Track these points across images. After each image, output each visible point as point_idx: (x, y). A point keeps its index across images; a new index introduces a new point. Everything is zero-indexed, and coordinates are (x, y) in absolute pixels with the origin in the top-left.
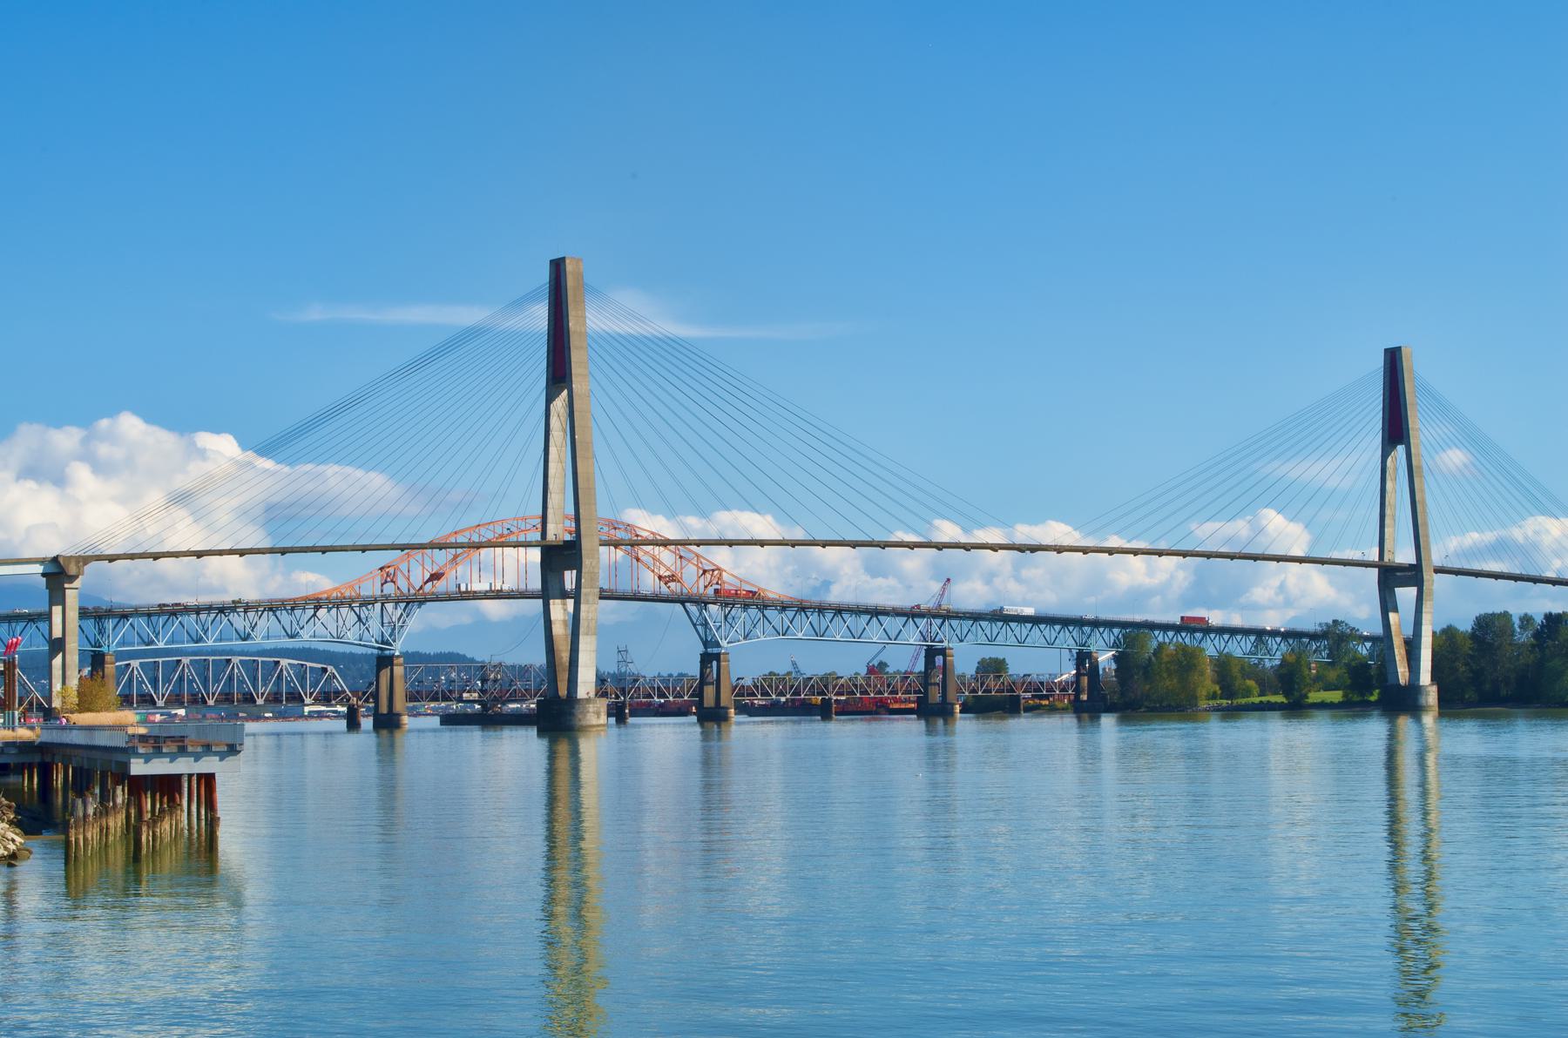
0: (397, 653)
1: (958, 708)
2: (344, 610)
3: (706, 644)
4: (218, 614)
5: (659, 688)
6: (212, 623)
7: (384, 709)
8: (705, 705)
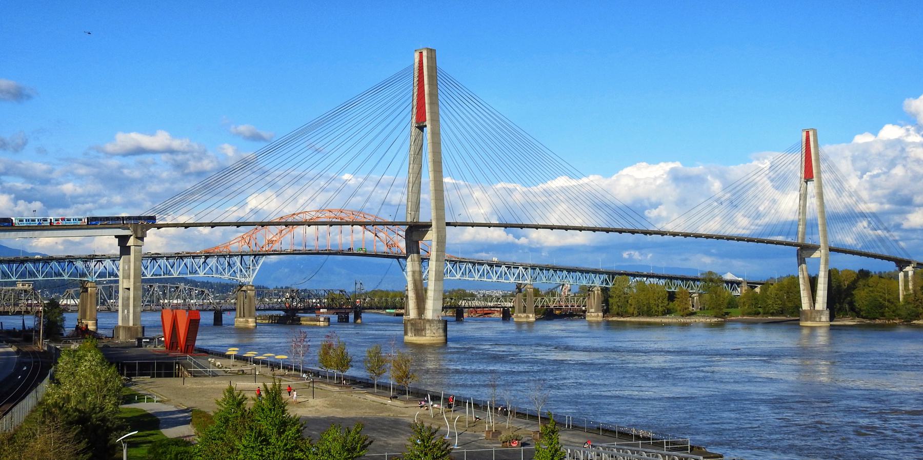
2: (222, 260)
4: (152, 260)
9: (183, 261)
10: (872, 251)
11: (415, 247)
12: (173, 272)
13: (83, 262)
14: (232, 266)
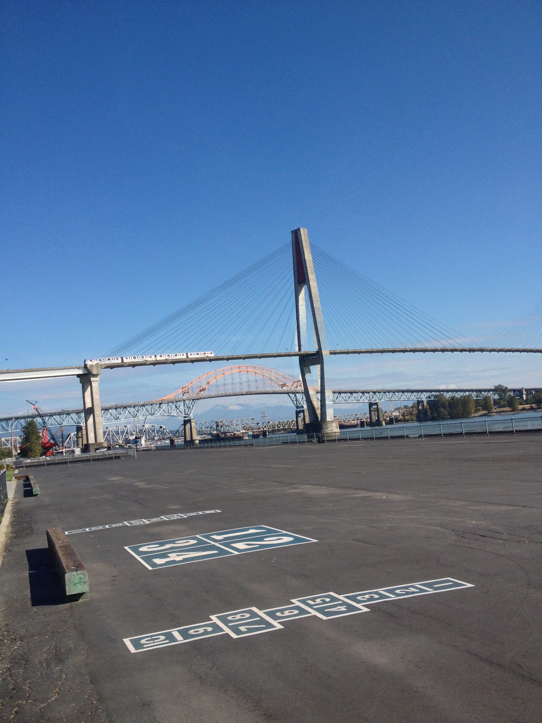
1: (384, 423)
2: (171, 404)
3: (297, 407)
4: (123, 409)
5: (285, 423)
6: (104, 414)
7: (188, 439)
8: (299, 429)
9: (127, 410)
13: (76, 413)
14: (178, 408)
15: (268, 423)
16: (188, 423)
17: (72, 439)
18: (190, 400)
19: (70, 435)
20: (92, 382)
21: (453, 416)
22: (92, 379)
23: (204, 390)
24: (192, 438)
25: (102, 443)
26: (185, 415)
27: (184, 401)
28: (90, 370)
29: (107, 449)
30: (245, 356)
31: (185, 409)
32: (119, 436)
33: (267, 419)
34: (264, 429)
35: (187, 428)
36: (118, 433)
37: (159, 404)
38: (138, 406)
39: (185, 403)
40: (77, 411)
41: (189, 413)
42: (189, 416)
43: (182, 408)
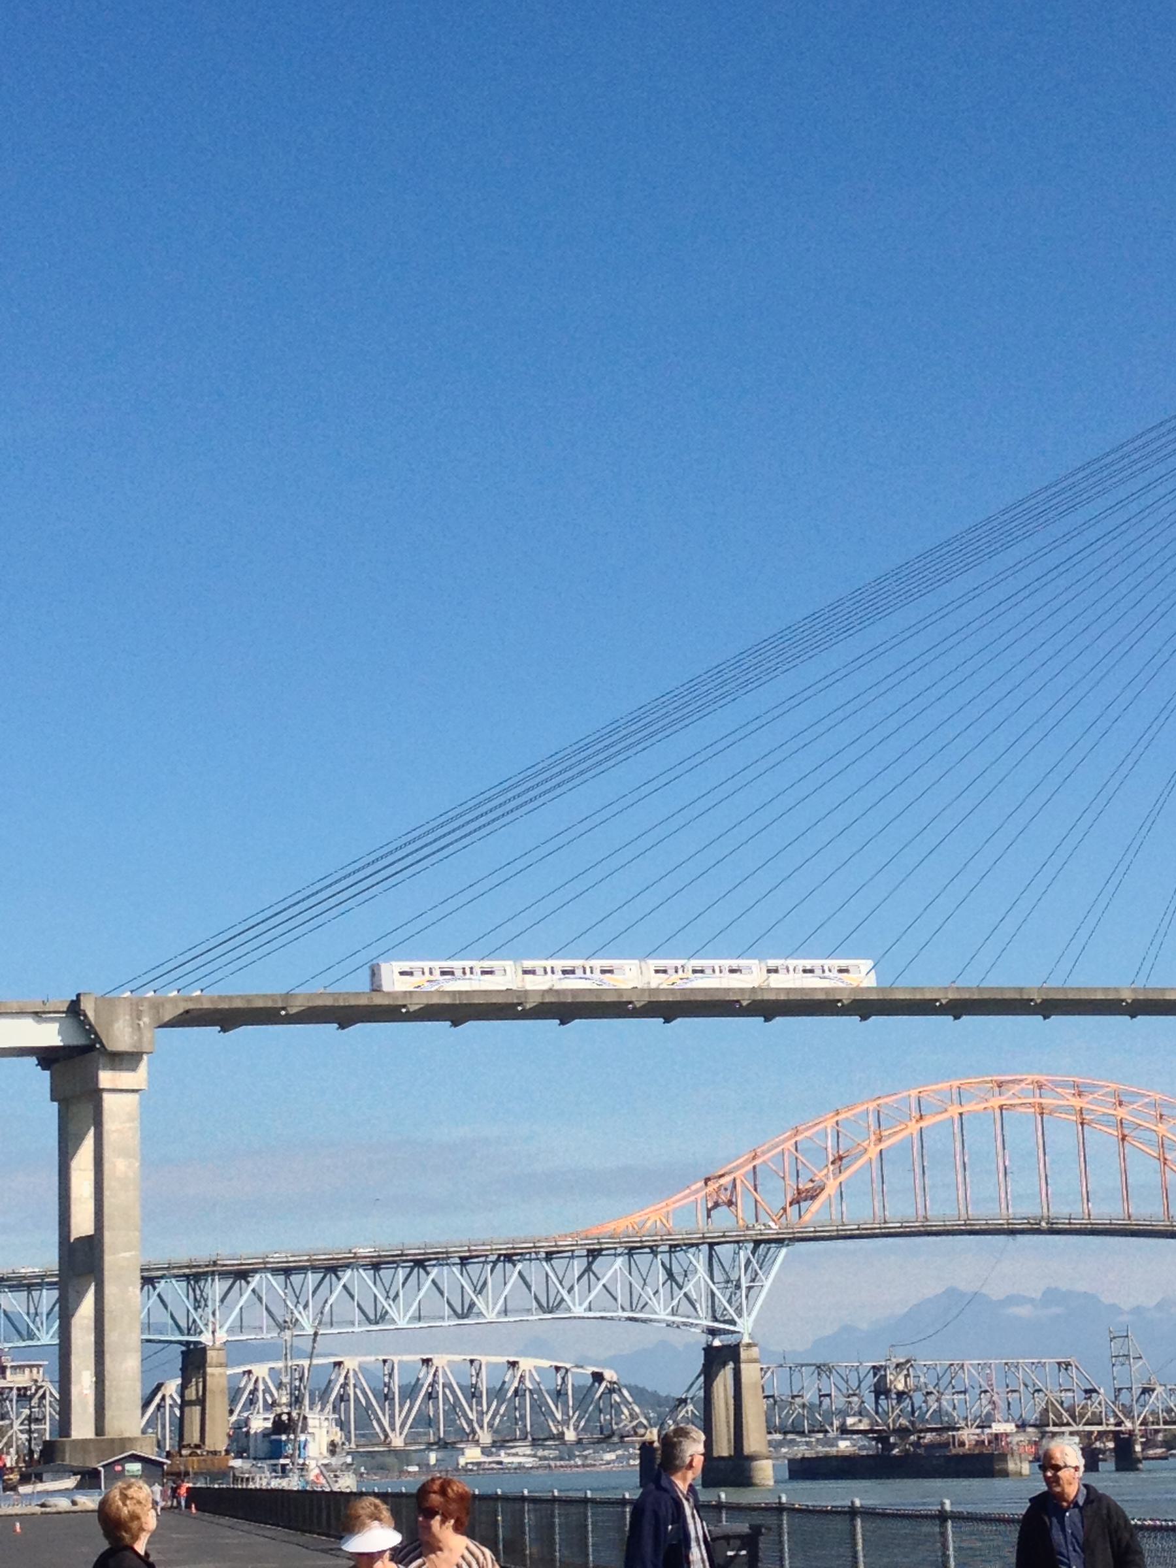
0: (746, 1340)
4: (412, 1268)
10: (17, 1323)
11: (88, 1110)
12: (570, 1304)
14: (680, 1279)
15: (1146, 1391)
16: (724, 1364)
17: (167, 1408)
18: (737, 1242)
19: (159, 1387)
20: (106, 1097)
21: (421, 1519)
22: (106, 1078)
23: (813, 1198)
24: (742, 1449)
25: (129, 1439)
26: (715, 1319)
27: (711, 1246)
28: (98, 1029)
29: (79, 1477)
30: (957, 996)
31: (713, 1294)
32: (392, 1417)
33: (1136, 1374)
34: (1119, 1424)
35: (721, 1389)
36: (473, 1394)
37: (585, 1253)
38: (482, 1259)
39: (715, 1260)
40: (187, 1267)
41: (731, 1311)
42: (732, 1328)
43: (698, 1282)
